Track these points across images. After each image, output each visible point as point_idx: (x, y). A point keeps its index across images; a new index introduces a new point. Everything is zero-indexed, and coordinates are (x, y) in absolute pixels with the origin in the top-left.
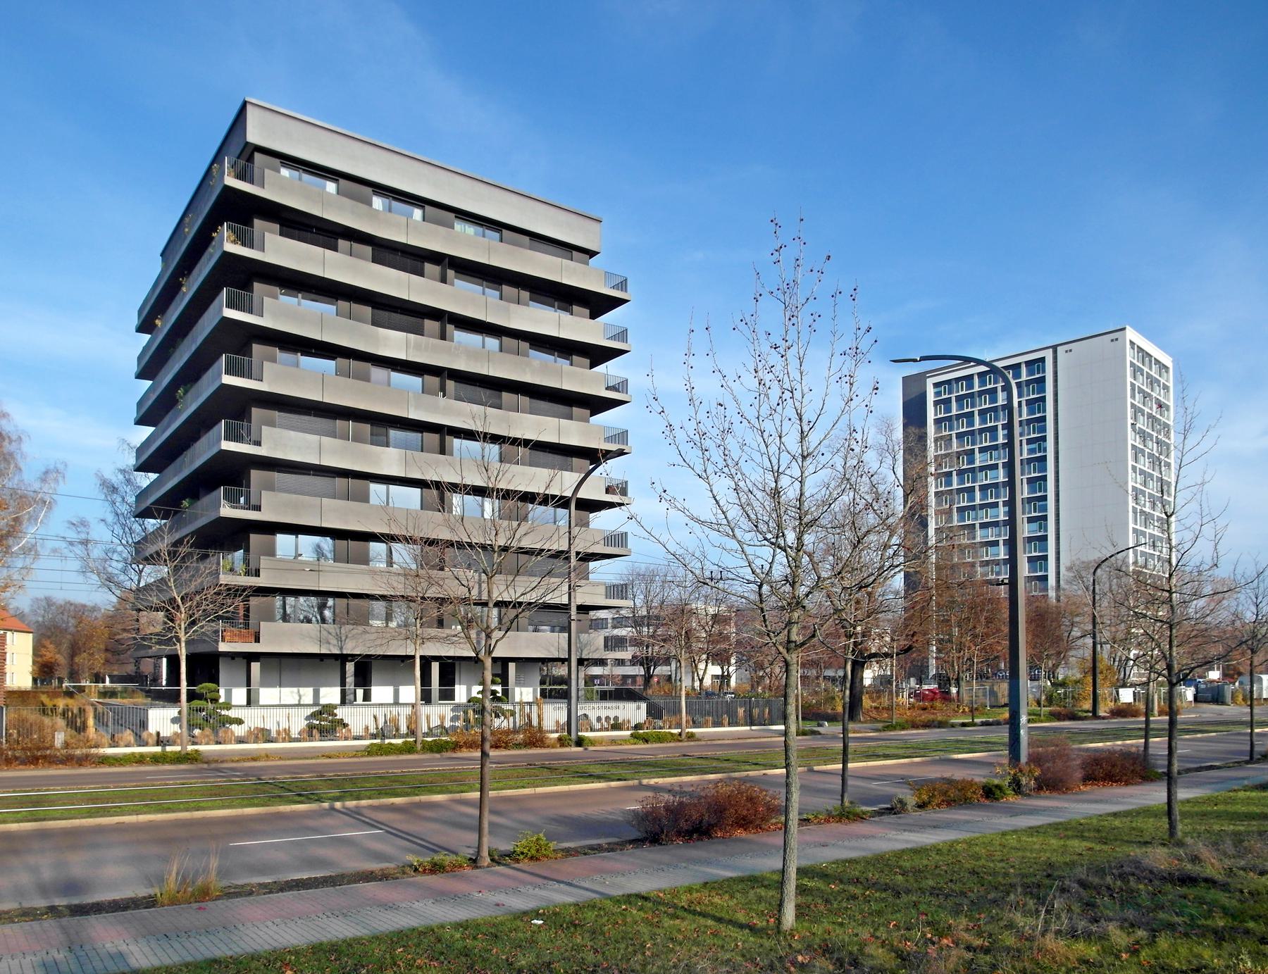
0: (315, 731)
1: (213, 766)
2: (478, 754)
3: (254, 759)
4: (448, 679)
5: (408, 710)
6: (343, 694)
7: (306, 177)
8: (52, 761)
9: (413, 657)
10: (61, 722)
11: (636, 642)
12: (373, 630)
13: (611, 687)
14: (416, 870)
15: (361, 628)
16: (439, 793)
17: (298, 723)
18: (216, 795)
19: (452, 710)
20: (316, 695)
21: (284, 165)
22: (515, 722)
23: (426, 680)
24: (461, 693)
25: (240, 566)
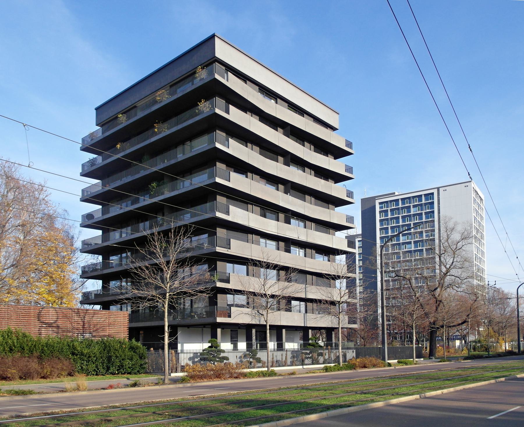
9: (338, 328)
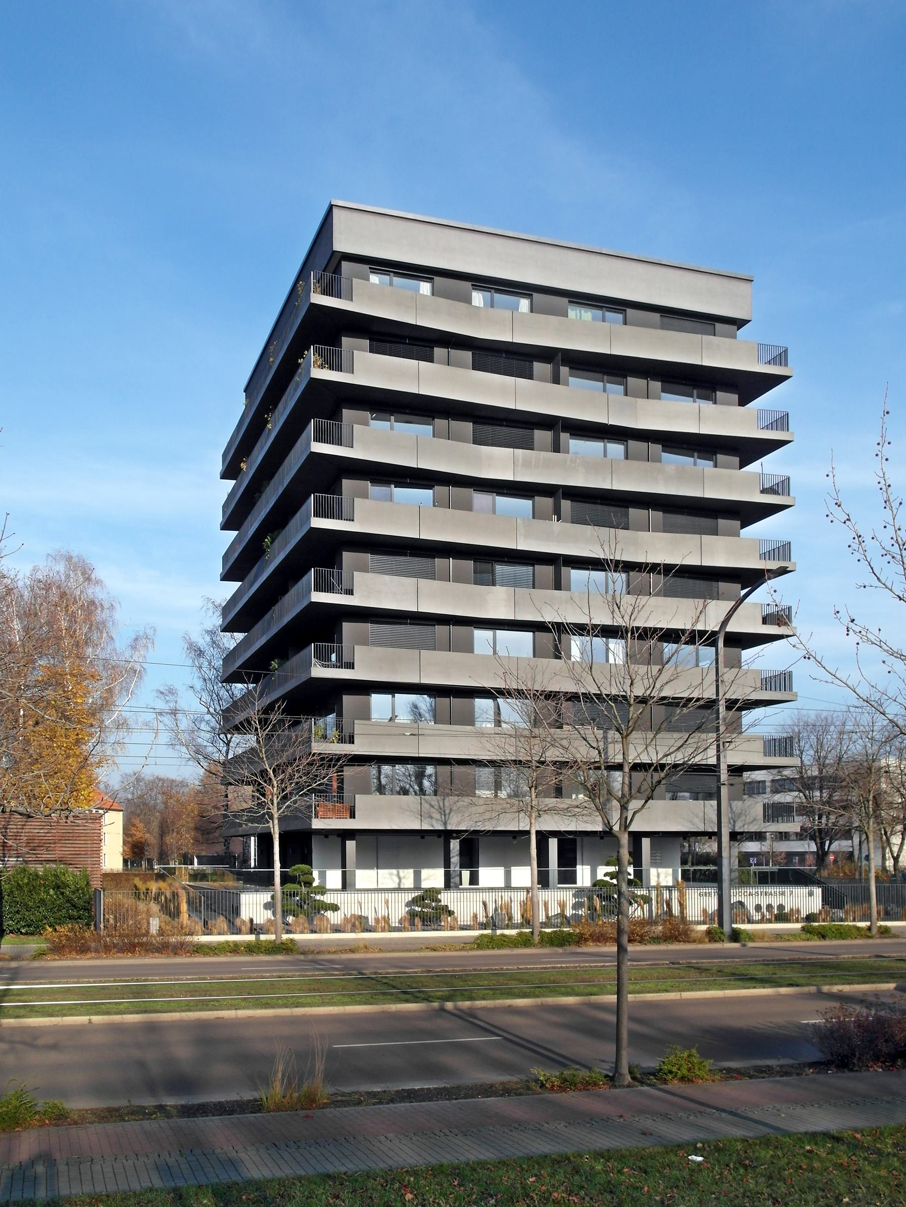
0: (417, 920)
1: (310, 957)
2: (615, 949)
3: (352, 951)
4: (568, 859)
5: (522, 896)
6: (448, 876)
7: (397, 280)
8: (149, 948)
9: (528, 833)
10: (155, 907)
11: (805, 810)
12: (481, 802)
13: (771, 868)
14: (542, 1086)
15: (467, 800)
16: (568, 994)
17: (398, 909)
18: (315, 990)
19: (574, 896)
20: (417, 877)
21: (373, 271)
22: (650, 911)
23: (543, 859)
24: (584, 875)
25: (332, 733)
